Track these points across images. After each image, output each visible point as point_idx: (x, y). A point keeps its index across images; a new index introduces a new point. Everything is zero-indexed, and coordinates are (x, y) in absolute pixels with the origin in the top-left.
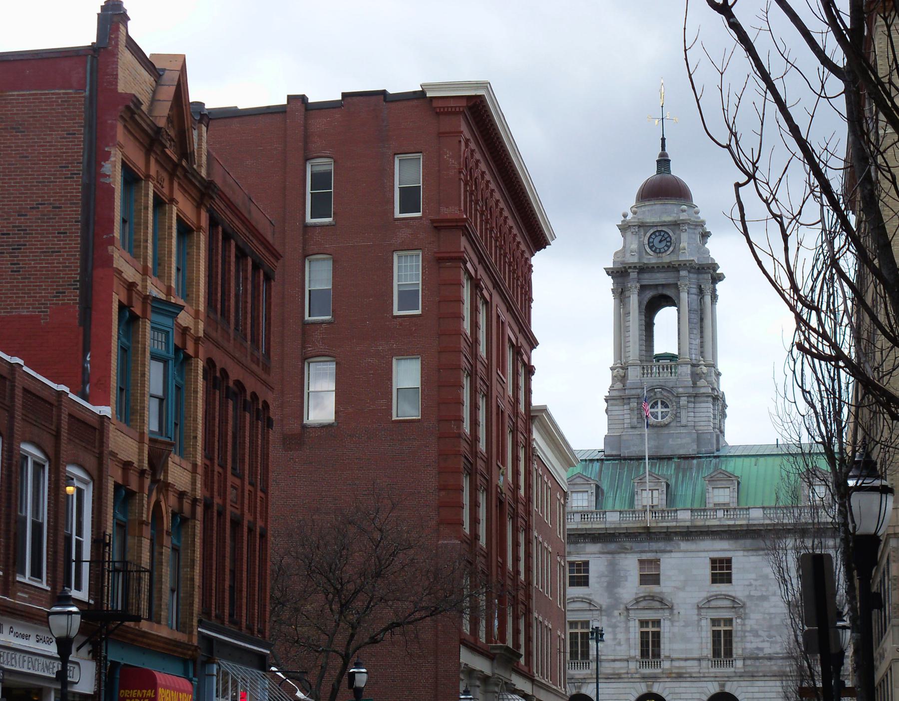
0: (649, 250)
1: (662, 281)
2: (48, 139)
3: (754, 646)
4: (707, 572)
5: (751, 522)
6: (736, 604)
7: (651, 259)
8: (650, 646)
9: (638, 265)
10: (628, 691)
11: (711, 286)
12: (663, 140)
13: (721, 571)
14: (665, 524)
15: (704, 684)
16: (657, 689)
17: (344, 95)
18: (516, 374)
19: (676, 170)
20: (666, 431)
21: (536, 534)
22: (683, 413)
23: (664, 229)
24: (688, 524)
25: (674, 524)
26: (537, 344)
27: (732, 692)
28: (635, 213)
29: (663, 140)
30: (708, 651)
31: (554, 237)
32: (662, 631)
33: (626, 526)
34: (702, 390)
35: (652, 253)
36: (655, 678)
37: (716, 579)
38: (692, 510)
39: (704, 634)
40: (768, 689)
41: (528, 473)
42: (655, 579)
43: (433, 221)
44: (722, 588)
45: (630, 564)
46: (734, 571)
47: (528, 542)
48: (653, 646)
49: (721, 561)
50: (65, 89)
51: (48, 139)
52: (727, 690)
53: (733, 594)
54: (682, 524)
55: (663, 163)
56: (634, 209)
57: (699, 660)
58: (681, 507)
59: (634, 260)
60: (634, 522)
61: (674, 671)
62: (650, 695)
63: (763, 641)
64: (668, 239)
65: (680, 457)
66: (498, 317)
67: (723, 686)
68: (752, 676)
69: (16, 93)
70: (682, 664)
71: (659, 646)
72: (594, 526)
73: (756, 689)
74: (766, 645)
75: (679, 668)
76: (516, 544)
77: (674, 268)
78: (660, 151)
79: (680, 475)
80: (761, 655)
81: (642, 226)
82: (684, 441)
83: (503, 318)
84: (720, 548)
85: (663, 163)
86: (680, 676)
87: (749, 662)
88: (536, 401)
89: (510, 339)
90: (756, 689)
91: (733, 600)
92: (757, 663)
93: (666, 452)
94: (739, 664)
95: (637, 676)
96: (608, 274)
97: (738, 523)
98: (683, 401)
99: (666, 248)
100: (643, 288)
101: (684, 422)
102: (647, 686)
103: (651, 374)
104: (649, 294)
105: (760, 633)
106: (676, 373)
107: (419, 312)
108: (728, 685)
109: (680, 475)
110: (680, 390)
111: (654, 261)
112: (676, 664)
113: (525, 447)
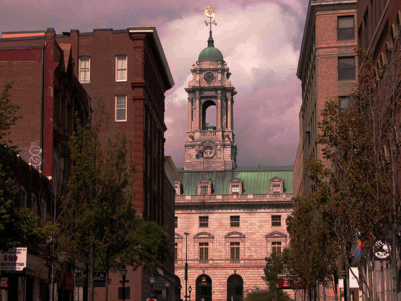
0: (204, 81)
1: (210, 95)
2: (28, 79)
3: (249, 254)
4: (228, 222)
5: (248, 200)
6: (242, 236)
7: (205, 84)
8: (204, 254)
9: (199, 88)
10: (194, 273)
11: (231, 97)
12: (211, 32)
13: (235, 221)
14: (211, 201)
15: (227, 271)
16: (206, 273)
17: (94, 30)
18: (159, 142)
19: (217, 45)
20: (211, 160)
21: (165, 209)
22: (219, 152)
23: (212, 72)
24: (221, 201)
25: (215, 201)
26: (167, 129)
27: (239, 274)
28: (198, 65)
29: (211, 32)
30: (229, 256)
31: (174, 84)
32: (178, 248)
33: (194, 202)
34: (227, 143)
35: (205, 82)
36: (207, 268)
37: (232, 225)
38: (223, 195)
39: (196, 249)
40: (255, 273)
41: (163, 183)
42: (206, 225)
43: (132, 84)
44: (235, 229)
45: (195, 218)
46: (240, 221)
47: (162, 212)
48: (236, 254)
49: (235, 217)
50: (33, 60)
51: (28, 79)
52: (206, 273)
53: (240, 232)
54: (218, 201)
55: (211, 42)
56: (198, 63)
57: (225, 260)
58: (218, 193)
59: (198, 85)
60: (197, 200)
61: (214, 265)
62: (204, 275)
63: (253, 252)
64: (213, 76)
65: (217, 172)
66: (154, 120)
67: (235, 271)
68: (248, 267)
69: (16, 62)
70: (218, 262)
71: (208, 254)
72: (180, 202)
73: (250, 273)
74: (254, 254)
75: (216, 263)
76: (159, 213)
77: (215, 89)
78: (209, 36)
79: (217, 180)
80: (252, 258)
81: (201, 71)
82: (219, 165)
83: (156, 120)
84: (235, 212)
85: (211, 42)
86: (216, 267)
87: (246, 261)
88: (166, 154)
89: (158, 129)
90: (250, 273)
91: (240, 234)
92: (250, 262)
93: (211, 170)
94: (242, 262)
95: (199, 267)
96: (186, 91)
97: (243, 201)
98: (219, 147)
99: (212, 80)
100: (201, 98)
101: (219, 156)
102: (234, 271)
103: (205, 135)
104: (203, 101)
105: (252, 248)
106: (215, 135)
107: (126, 120)
108: (238, 271)
109: (217, 180)
110: (218, 142)
111: (206, 86)
112: (215, 262)
113: (161, 173)
